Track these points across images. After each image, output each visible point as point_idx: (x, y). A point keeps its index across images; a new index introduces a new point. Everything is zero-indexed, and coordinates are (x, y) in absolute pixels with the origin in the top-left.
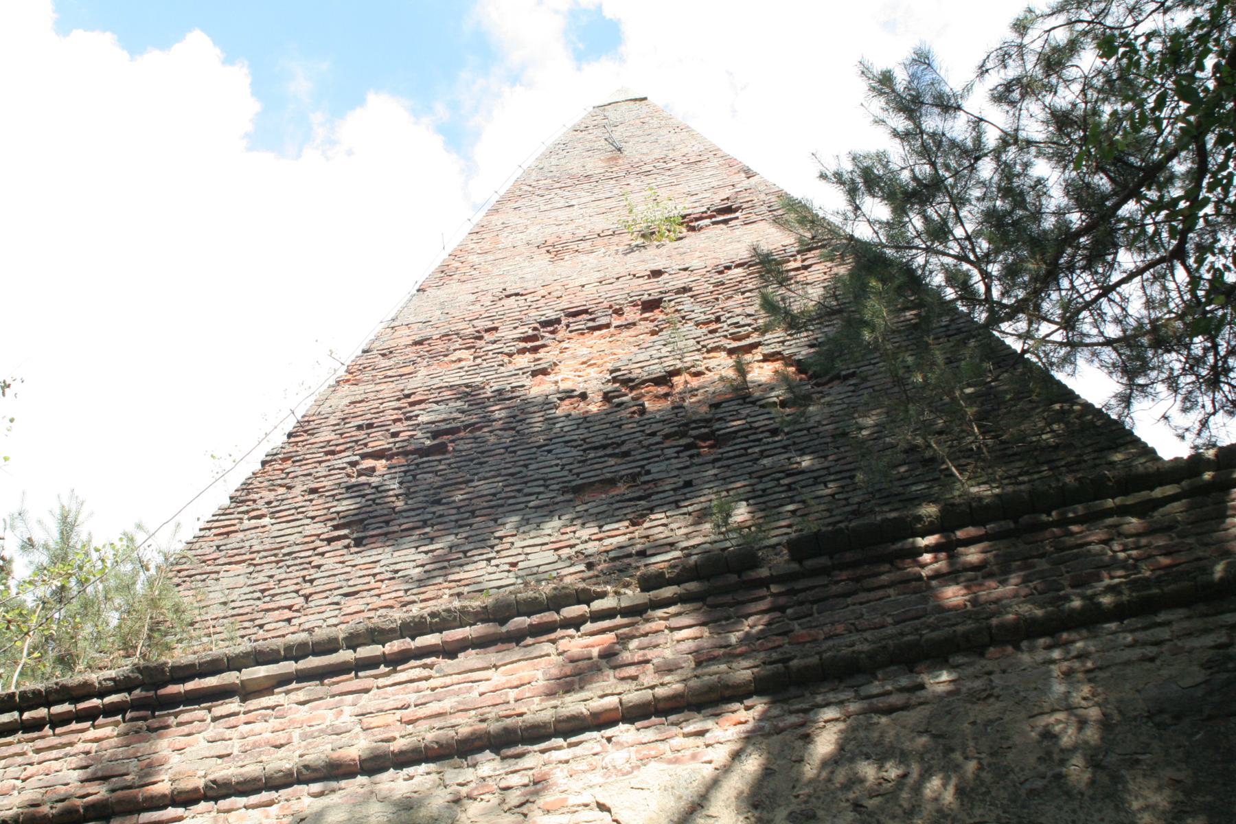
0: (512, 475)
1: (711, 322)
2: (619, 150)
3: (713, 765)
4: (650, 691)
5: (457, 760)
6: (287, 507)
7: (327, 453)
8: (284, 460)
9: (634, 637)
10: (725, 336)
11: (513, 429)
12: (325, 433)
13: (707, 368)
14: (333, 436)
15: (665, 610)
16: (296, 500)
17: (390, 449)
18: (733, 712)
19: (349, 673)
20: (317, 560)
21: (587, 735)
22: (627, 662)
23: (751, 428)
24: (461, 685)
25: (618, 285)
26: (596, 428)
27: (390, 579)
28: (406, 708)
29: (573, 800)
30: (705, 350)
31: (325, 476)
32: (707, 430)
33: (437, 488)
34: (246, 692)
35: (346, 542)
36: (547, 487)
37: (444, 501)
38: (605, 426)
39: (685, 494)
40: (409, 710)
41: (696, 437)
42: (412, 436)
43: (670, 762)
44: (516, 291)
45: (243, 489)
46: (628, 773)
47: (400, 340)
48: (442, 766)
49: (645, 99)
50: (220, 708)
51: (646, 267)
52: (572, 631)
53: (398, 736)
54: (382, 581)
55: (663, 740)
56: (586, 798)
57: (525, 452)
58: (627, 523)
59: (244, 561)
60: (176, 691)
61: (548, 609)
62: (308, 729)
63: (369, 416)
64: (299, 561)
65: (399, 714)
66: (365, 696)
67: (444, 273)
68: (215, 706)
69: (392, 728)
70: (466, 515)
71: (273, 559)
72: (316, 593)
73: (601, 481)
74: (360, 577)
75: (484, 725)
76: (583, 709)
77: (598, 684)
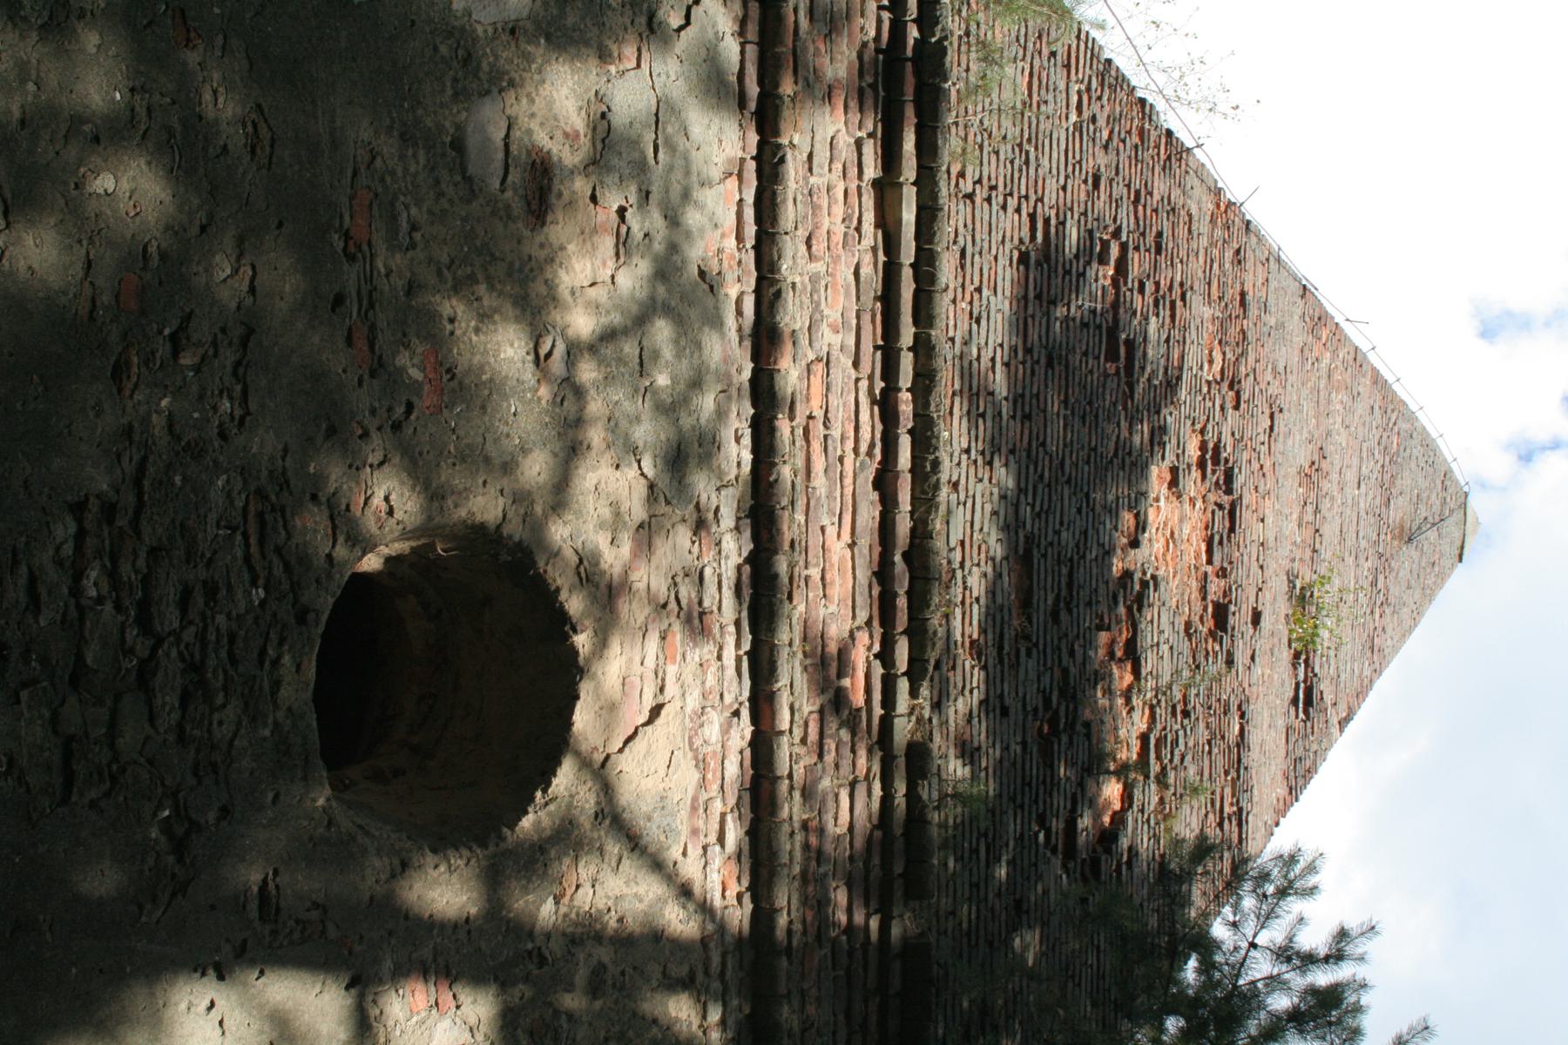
0: (1062, 464)
2: (1410, 539)
3: (680, 858)
4: (786, 773)
5: (749, 503)
7: (1138, 193)
8: (1141, 132)
9: (854, 734)
10: (1165, 729)
11: (1116, 454)
14: (1157, 197)
16: (1090, 160)
17: (1126, 283)
18: (739, 879)
19: (883, 338)
20: (1012, 203)
21: (747, 683)
26: (1094, 571)
28: (824, 423)
29: (672, 670)
31: (1111, 196)
32: (1062, 726)
33: (1067, 360)
34: (886, 189)
35: (1027, 240)
36: (1039, 515)
38: (1094, 582)
39: (994, 710)
41: (1056, 712)
43: (695, 799)
44: (1276, 428)
46: (691, 744)
48: (745, 483)
49: (1460, 560)
52: (877, 648)
53: (794, 424)
54: (971, 303)
55: (722, 787)
56: (672, 689)
57: (1086, 476)
58: (975, 636)
59: (1030, 95)
60: (905, 88)
61: (910, 619)
62: (823, 283)
63: (1170, 245)
64: (1016, 175)
65: (819, 413)
66: (850, 363)
67: (1319, 320)
68: (875, 144)
71: (1026, 136)
72: (974, 209)
73: (1031, 586)
74: (981, 270)
75: (786, 547)
76: (783, 681)
77: (806, 691)
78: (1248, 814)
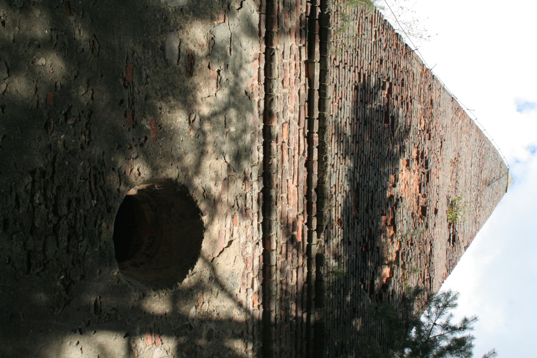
0: (369, 158)
1: (412, 241)
2: (489, 185)
3: (238, 293)
4: (275, 264)
5: (262, 171)
6: (377, 50)
7: (395, 66)
8: (397, 45)
10: (404, 249)
12: (404, 63)
13: (393, 243)
14: (402, 67)
15: (306, 265)
16: (379, 54)
17: (391, 96)
19: (308, 115)
20: (352, 69)
21: (261, 233)
22: (288, 249)
23: (366, 269)
24: (293, 170)
25: (435, 194)
26: (380, 195)
27: (338, 107)
28: (288, 144)
29: (236, 229)
30: (401, 240)
31: (386, 66)
32: (369, 248)
34: (309, 64)
35: (357, 82)
37: (365, 127)
38: (380, 199)
39: (346, 243)
40: (287, 145)
41: (367, 243)
42: (394, 107)
43: (243, 273)
44: (443, 146)
45: (388, 26)
46: (242, 254)
47: (434, 93)
49: (506, 192)
50: (304, 51)
51: (440, 207)
52: (306, 221)
53: (278, 144)
54: (338, 103)
55: (253, 269)
56: (235, 235)
58: (340, 217)
59: (359, 32)
62: (288, 96)
63: (407, 83)
64: (354, 59)
65: (286, 141)
66: (297, 124)
67: (458, 109)
68: (305, 48)
69: (281, 138)
70: (357, 139)
71: (357, 46)
74: (342, 92)
76: (274, 233)
77: (281, 236)
78: (433, 279)
